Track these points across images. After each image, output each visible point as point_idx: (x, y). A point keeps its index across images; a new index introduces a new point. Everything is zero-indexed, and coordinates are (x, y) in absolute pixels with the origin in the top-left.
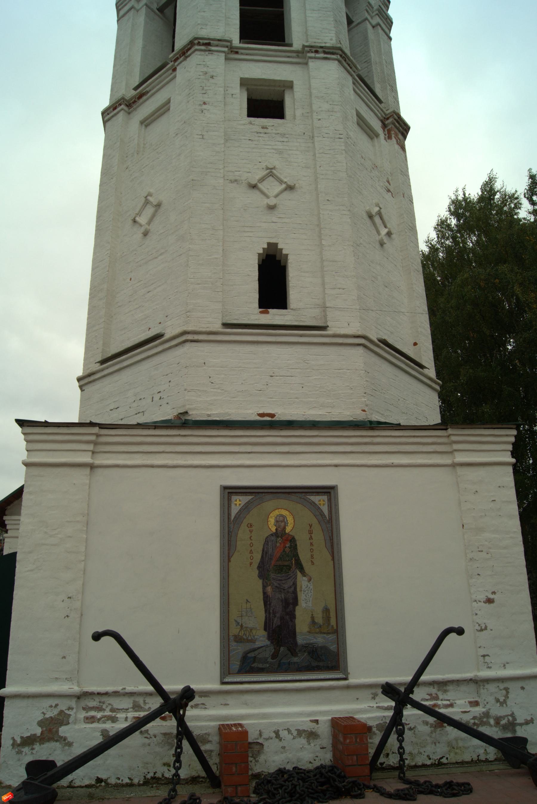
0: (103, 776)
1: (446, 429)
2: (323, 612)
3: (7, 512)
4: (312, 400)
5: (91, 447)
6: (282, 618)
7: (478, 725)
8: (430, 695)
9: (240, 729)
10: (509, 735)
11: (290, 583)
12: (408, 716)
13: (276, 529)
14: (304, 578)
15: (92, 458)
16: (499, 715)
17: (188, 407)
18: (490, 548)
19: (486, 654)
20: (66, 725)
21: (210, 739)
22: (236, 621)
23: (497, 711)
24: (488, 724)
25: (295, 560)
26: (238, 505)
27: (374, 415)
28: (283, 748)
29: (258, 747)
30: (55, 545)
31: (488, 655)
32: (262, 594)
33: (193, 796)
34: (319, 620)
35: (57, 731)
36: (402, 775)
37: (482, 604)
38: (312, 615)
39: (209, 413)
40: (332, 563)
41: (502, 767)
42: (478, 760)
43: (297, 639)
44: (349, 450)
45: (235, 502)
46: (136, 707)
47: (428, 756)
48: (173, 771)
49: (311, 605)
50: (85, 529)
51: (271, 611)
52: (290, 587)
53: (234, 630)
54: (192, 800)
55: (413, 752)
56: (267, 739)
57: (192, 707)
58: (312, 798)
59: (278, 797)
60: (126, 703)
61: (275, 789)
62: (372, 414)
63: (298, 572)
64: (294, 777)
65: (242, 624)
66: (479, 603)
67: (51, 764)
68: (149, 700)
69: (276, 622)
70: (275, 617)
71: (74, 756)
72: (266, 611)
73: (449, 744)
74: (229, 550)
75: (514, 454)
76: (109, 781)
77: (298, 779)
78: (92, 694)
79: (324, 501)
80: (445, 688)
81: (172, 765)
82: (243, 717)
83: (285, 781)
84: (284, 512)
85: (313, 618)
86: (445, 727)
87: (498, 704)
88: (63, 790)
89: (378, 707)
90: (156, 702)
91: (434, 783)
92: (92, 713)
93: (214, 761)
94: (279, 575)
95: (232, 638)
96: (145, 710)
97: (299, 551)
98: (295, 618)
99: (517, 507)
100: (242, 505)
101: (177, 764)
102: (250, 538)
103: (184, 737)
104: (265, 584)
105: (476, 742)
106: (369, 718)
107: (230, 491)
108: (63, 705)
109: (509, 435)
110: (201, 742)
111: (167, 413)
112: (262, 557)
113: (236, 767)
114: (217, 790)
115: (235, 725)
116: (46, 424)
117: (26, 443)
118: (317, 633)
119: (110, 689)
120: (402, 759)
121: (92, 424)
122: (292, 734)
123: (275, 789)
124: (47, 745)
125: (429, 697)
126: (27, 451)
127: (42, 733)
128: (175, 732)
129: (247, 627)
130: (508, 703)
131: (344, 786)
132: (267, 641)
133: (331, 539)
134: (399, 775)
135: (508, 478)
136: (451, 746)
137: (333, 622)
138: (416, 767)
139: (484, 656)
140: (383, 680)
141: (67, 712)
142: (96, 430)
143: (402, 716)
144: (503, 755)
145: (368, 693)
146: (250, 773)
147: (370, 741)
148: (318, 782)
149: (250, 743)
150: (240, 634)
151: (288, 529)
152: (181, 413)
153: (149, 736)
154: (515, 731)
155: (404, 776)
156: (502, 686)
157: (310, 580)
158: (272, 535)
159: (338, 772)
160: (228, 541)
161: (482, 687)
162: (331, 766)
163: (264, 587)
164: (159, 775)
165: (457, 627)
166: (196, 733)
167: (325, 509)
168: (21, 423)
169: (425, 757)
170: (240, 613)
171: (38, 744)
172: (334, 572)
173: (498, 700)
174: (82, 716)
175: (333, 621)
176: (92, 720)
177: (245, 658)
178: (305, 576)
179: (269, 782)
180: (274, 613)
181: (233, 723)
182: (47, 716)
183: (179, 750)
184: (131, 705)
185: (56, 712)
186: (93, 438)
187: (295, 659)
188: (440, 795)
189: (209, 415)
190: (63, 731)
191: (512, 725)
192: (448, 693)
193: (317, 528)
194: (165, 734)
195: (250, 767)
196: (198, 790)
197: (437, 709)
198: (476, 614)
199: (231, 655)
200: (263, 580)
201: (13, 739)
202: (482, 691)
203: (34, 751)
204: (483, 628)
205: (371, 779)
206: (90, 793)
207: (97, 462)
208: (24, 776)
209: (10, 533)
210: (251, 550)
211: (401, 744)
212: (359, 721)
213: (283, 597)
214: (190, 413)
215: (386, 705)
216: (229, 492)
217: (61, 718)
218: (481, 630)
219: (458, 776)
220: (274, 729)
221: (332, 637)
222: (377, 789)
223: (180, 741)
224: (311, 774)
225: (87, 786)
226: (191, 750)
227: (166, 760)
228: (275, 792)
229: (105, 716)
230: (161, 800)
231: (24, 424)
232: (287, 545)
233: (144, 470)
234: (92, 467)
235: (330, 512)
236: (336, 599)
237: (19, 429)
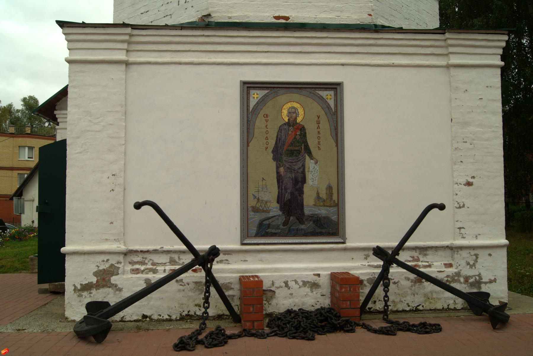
0: (148, 314)
1: (444, 34)
2: (327, 189)
3: (57, 108)
4: (323, 4)
5: (125, 46)
6: (292, 194)
7: (450, 282)
8: (413, 257)
9: (256, 279)
10: (475, 290)
11: (300, 164)
12: (393, 273)
13: (289, 120)
14: (312, 161)
15: (127, 56)
16: (468, 275)
17: (210, 9)
18: (474, 140)
19: (462, 227)
20: (116, 275)
21: (232, 287)
22: (253, 195)
23: (467, 271)
24: (459, 281)
25: (305, 146)
27: (379, 20)
28: (291, 294)
29: (271, 293)
30: (99, 131)
31: (463, 228)
32: (275, 174)
33: (218, 328)
34: (323, 195)
35: (110, 280)
36: (386, 317)
37: (463, 186)
39: (230, 15)
40: (336, 148)
41: (466, 314)
42: (448, 308)
44: (355, 51)
46: (172, 262)
47: (407, 304)
48: (203, 310)
49: (316, 183)
50: (124, 118)
51: (283, 188)
52: (300, 168)
53: (252, 202)
54: (218, 331)
55: (396, 300)
56: (278, 288)
57: (218, 262)
58: (313, 331)
59: (286, 330)
60: (164, 259)
61: (284, 324)
62: (377, 18)
63: (307, 156)
64: (299, 316)
66: (460, 186)
67: (106, 304)
68: (182, 256)
69: (287, 196)
70: (287, 192)
71: (123, 298)
73: (425, 295)
74: (248, 136)
75: (503, 58)
76: (152, 317)
77: (303, 317)
78: (136, 252)
79: (331, 95)
80: (425, 253)
81: (202, 306)
82: (259, 270)
83: (292, 319)
85: (318, 194)
86: (423, 282)
87: (468, 267)
88: (117, 324)
89: (369, 265)
90: (188, 258)
91: (411, 323)
92: (137, 266)
93: (235, 303)
95: (250, 209)
96: (179, 265)
98: (303, 194)
99: (501, 105)
100: (259, 99)
101: (206, 305)
103: (212, 285)
104: (278, 165)
105: (448, 294)
106: (361, 274)
107: (249, 85)
108: (113, 260)
109: (500, 41)
110: (225, 289)
111: (192, 16)
112: (276, 142)
113: (253, 307)
114: (238, 324)
115: (252, 276)
116: (84, 25)
117: (67, 42)
118: (321, 206)
119: (151, 248)
120: (386, 305)
121: (125, 25)
122: (298, 284)
123: (284, 324)
124: (101, 290)
125: (411, 259)
126: (69, 49)
127: (97, 281)
128: (204, 281)
129: (262, 200)
130: (477, 266)
131: (339, 323)
133: (336, 129)
134: (383, 317)
135: (495, 79)
136: (427, 297)
137: (335, 197)
138: (397, 311)
139: (460, 228)
140: (374, 244)
141: (116, 265)
142: (129, 30)
143: (389, 272)
144: (469, 305)
145: (362, 254)
146: (264, 312)
147: (361, 291)
148: (318, 320)
149: (264, 290)
150: (257, 206)
151: (299, 120)
152: (204, 16)
153: (183, 284)
154: (480, 288)
155: (387, 318)
156: (473, 252)
157: (316, 163)
158: (285, 124)
159: (334, 313)
160: (247, 129)
161: (456, 253)
162: (329, 308)
163: (278, 168)
164: (192, 313)
165: (439, 203)
166: (221, 282)
167: (332, 103)
168: (62, 24)
169: (405, 304)
171: (94, 289)
173: (468, 264)
174: (129, 269)
175: (335, 196)
176: (137, 271)
177: (261, 225)
178: (312, 159)
179: (279, 319)
180: (286, 189)
181: (250, 275)
182: (101, 268)
183: (207, 294)
184: (168, 261)
185: (107, 265)
186: (127, 38)
187: (303, 227)
188: (415, 332)
189: (230, 18)
190: (114, 279)
191: (478, 283)
192: (428, 257)
193: (324, 120)
194: (196, 283)
195: (264, 308)
196: (223, 324)
197: (417, 268)
198: (457, 194)
199: (249, 222)
200: (277, 162)
201: (74, 285)
202: (456, 256)
203: (92, 295)
204: (461, 206)
205: (360, 319)
206: (138, 326)
207: (131, 59)
208: (85, 312)
209: (61, 125)
210: (267, 137)
211: (386, 294)
212: (353, 275)
214: (213, 15)
215: (375, 264)
216: (248, 86)
217: (112, 270)
218: (460, 207)
219: (431, 319)
220: (284, 280)
221: (334, 210)
222: (365, 326)
223: (208, 287)
224: (313, 314)
225: (135, 321)
226: (217, 295)
227: (197, 302)
228: (284, 326)
229: (147, 269)
230: (194, 331)
231: (64, 25)
232: (298, 133)
233: (173, 67)
234: (127, 64)
235: (336, 105)
236: (338, 178)
237: (60, 30)
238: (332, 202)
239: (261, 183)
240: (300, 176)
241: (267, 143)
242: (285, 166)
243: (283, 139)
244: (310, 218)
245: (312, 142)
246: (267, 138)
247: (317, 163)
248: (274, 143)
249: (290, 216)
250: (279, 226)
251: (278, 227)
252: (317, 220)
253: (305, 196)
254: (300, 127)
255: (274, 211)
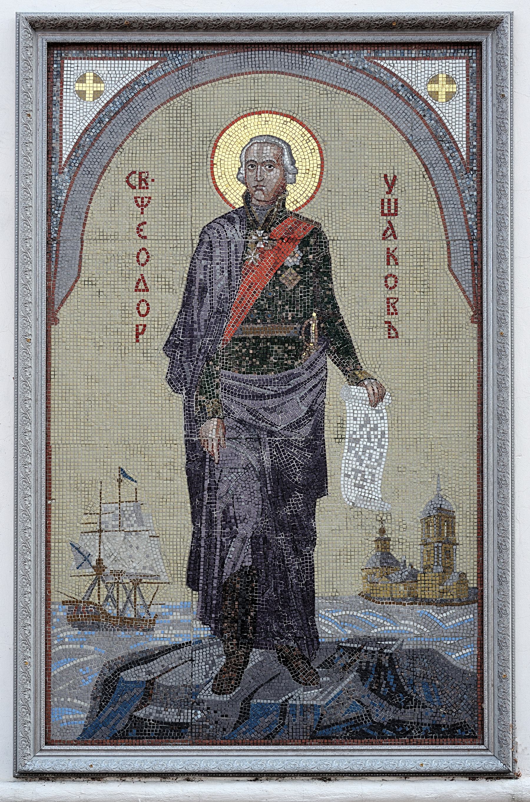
2: (426, 522)
6: (259, 543)
13: (247, 197)
25: (321, 319)
26: (89, 97)
32: (182, 448)
34: (410, 550)
38: (382, 531)
43: (318, 620)
45: (79, 87)
51: (217, 514)
53: (72, 583)
65: (99, 561)
69: (238, 555)
70: (233, 535)
72: (195, 515)
79: (450, 80)
84: (274, 126)
85: (383, 542)
94: (254, 377)
95: (60, 613)
97: (336, 286)
98: (313, 543)
100: (105, 99)
102: (139, 230)
112: (186, 304)
129: (119, 574)
132: (198, 623)
133: (476, 240)
137: (464, 561)
151: (295, 197)
157: (377, 399)
158: (228, 218)
163: (193, 422)
170: (95, 518)
172: (480, 369)
175: (453, 563)
177: (109, 687)
180: (229, 521)
187: (308, 696)
199: (54, 672)
213: (267, 464)
221: (461, 617)
232: (290, 261)
235: (476, 127)
238: (452, 581)
239: (111, 492)
240: (299, 458)
241: (143, 309)
242: (229, 412)
243: (217, 288)
244: (346, 659)
245: (356, 298)
246: (141, 285)
247: (382, 398)
248: (174, 302)
249: (254, 644)
250: (194, 691)
251: (191, 698)
252: (379, 666)
253: (321, 555)
254: (301, 233)
255: (177, 624)
